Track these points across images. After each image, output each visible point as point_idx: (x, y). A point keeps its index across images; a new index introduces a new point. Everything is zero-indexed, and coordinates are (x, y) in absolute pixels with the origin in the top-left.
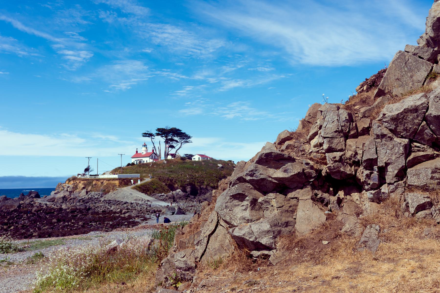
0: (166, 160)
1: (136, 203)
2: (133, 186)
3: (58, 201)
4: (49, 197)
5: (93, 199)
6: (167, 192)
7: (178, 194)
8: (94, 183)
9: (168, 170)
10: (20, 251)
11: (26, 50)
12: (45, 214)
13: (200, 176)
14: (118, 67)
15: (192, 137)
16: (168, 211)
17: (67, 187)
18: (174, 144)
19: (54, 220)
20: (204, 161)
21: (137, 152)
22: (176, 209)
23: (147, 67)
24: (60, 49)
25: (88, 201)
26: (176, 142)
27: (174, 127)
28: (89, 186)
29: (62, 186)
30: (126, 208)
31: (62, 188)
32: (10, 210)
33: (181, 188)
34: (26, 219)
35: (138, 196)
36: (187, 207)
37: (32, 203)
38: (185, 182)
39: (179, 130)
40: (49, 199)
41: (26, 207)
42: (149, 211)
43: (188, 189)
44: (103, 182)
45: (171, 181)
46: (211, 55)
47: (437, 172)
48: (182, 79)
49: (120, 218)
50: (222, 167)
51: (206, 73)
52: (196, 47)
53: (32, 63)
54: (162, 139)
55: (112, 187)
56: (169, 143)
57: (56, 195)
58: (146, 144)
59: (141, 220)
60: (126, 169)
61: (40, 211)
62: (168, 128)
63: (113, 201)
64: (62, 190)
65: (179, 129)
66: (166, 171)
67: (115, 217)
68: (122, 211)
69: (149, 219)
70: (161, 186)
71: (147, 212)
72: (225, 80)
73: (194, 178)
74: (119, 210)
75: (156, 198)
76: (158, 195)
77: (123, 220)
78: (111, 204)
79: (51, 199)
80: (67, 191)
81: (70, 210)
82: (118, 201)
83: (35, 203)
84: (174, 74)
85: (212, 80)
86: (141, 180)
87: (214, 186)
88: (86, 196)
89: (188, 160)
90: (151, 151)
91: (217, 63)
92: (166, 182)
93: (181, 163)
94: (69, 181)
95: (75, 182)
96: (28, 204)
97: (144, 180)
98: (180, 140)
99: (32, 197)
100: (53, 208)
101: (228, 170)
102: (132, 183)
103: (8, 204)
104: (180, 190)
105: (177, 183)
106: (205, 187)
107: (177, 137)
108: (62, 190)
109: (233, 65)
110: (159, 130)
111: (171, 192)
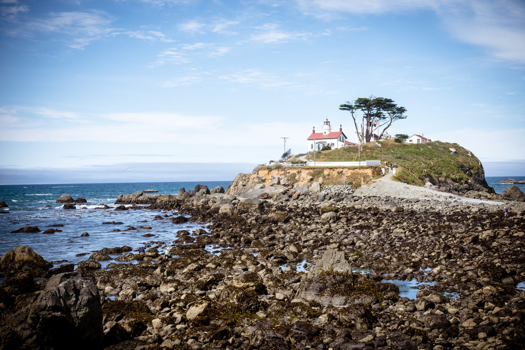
8: (326, 172)
21: (314, 131)
38: (422, 172)
47: (305, 156)
50: (455, 152)
58: (329, 121)
90: (339, 131)
94: (269, 170)
106: (443, 179)
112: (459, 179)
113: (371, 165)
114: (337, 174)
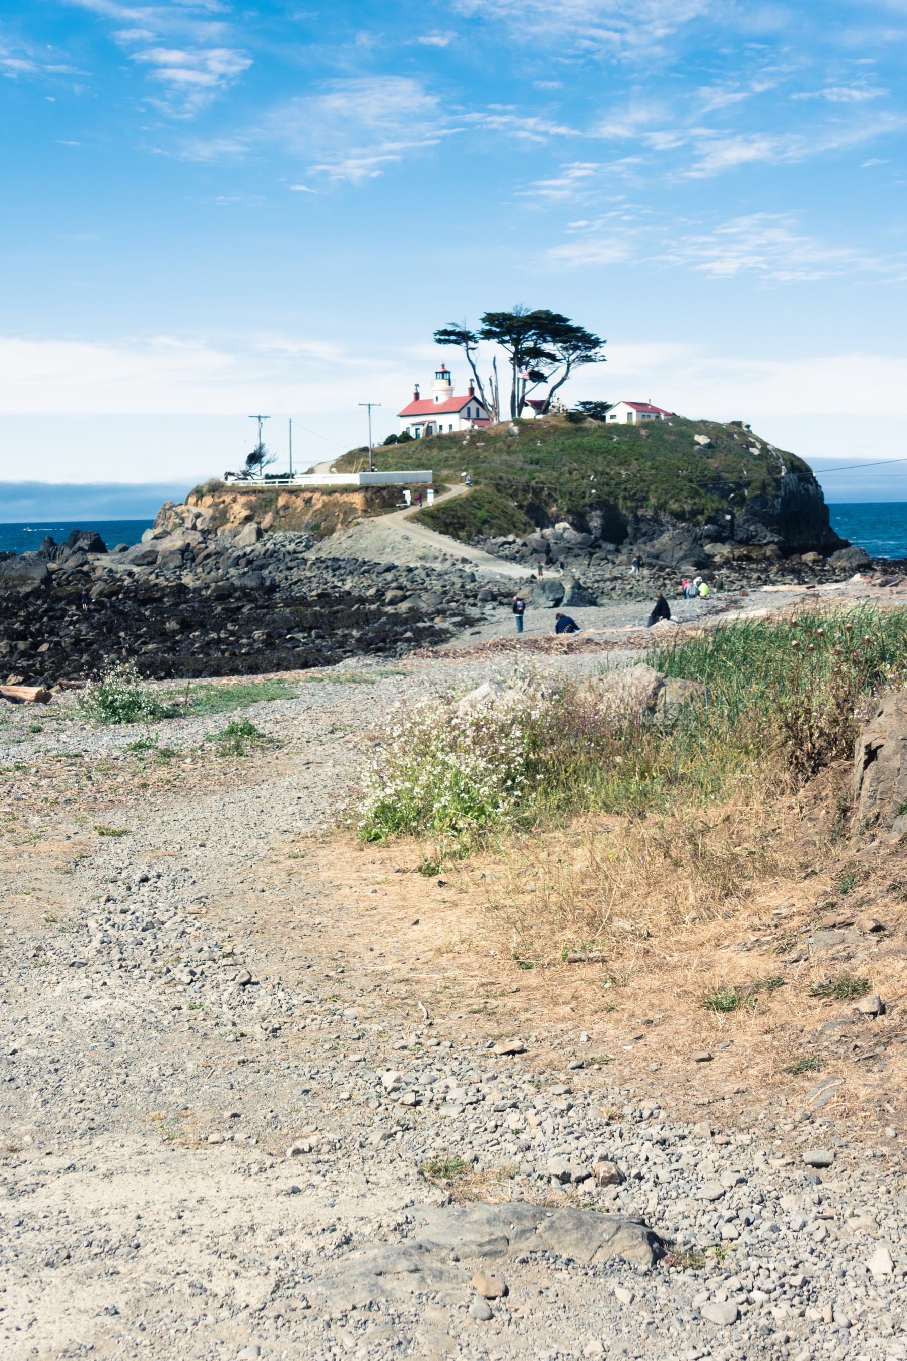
0: (518, 422)
1: (425, 568)
2: (415, 509)
3: (166, 563)
4: (136, 550)
5: (281, 556)
6: (525, 531)
7: (559, 538)
8: (281, 501)
9: (525, 457)
10: (170, 715)
11: (31, 54)
12: (135, 605)
13: (635, 476)
14: (335, 103)
15: (604, 342)
16: (539, 596)
17: (192, 516)
18: (544, 366)
19: (171, 625)
20: (645, 426)
21: (417, 395)
22: (568, 587)
23: (437, 100)
24: (141, 45)
25: (264, 561)
26: (549, 361)
27: (544, 308)
28: (265, 513)
29: (177, 513)
30: (394, 585)
31: (177, 521)
32: (18, 592)
33: (571, 518)
34: (77, 621)
35: (429, 543)
36: (597, 581)
37: (86, 568)
38: (584, 497)
39: (559, 318)
40: (136, 557)
41: (69, 583)
42: (475, 596)
43: (595, 522)
44: (311, 498)
45: (537, 492)
46: (658, 51)
48: (559, 137)
49: (384, 619)
50: (709, 446)
51: (640, 115)
52: (606, 21)
53: (52, 99)
54: (503, 352)
55: (341, 515)
56: (527, 364)
57: (159, 541)
58: (447, 369)
59: (455, 624)
60: (384, 454)
61: (116, 593)
62: (523, 313)
63: (348, 561)
64: (176, 526)
65: (559, 315)
66: (518, 460)
67: (366, 615)
68: (383, 594)
69: (479, 620)
70: (503, 511)
71: (467, 597)
72: (708, 139)
73: (613, 482)
74: (372, 591)
75: (488, 552)
76: (494, 541)
77: (395, 624)
78: (342, 571)
79: (144, 556)
80: (194, 527)
81: (214, 591)
82: (365, 562)
83: (94, 569)
84: (531, 122)
85: (662, 140)
86: (437, 492)
87: (684, 512)
88: (259, 545)
89: (591, 423)
90: (466, 393)
91: (682, 76)
92: (520, 497)
93: (566, 433)
95: (217, 500)
96: (72, 573)
97: (445, 490)
98: (565, 353)
99: (80, 549)
100: (156, 585)
101: (730, 456)
102: (409, 503)
103: (13, 573)
104: (568, 525)
105: (556, 500)
106: (650, 513)
107: (555, 341)
108: (176, 526)
109: (737, 84)
110: (490, 318)
111: (538, 530)
112: (690, 513)
113: (368, 482)
114: (303, 504)
